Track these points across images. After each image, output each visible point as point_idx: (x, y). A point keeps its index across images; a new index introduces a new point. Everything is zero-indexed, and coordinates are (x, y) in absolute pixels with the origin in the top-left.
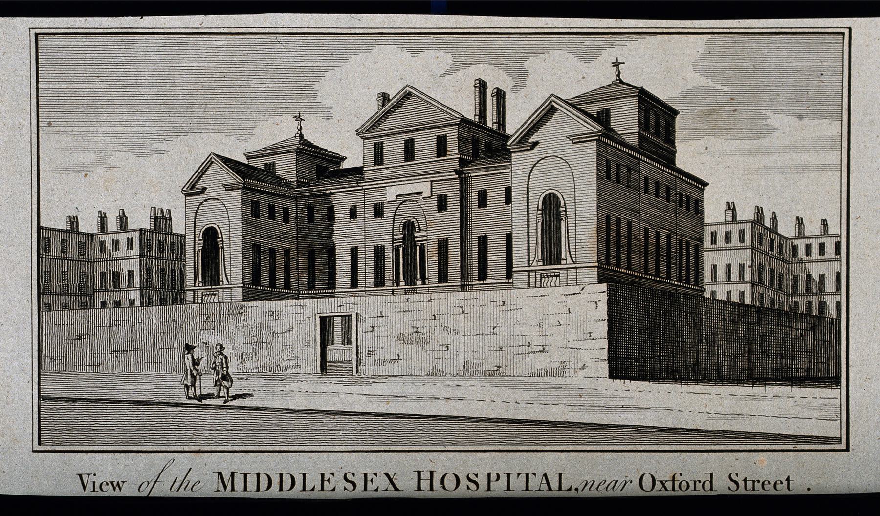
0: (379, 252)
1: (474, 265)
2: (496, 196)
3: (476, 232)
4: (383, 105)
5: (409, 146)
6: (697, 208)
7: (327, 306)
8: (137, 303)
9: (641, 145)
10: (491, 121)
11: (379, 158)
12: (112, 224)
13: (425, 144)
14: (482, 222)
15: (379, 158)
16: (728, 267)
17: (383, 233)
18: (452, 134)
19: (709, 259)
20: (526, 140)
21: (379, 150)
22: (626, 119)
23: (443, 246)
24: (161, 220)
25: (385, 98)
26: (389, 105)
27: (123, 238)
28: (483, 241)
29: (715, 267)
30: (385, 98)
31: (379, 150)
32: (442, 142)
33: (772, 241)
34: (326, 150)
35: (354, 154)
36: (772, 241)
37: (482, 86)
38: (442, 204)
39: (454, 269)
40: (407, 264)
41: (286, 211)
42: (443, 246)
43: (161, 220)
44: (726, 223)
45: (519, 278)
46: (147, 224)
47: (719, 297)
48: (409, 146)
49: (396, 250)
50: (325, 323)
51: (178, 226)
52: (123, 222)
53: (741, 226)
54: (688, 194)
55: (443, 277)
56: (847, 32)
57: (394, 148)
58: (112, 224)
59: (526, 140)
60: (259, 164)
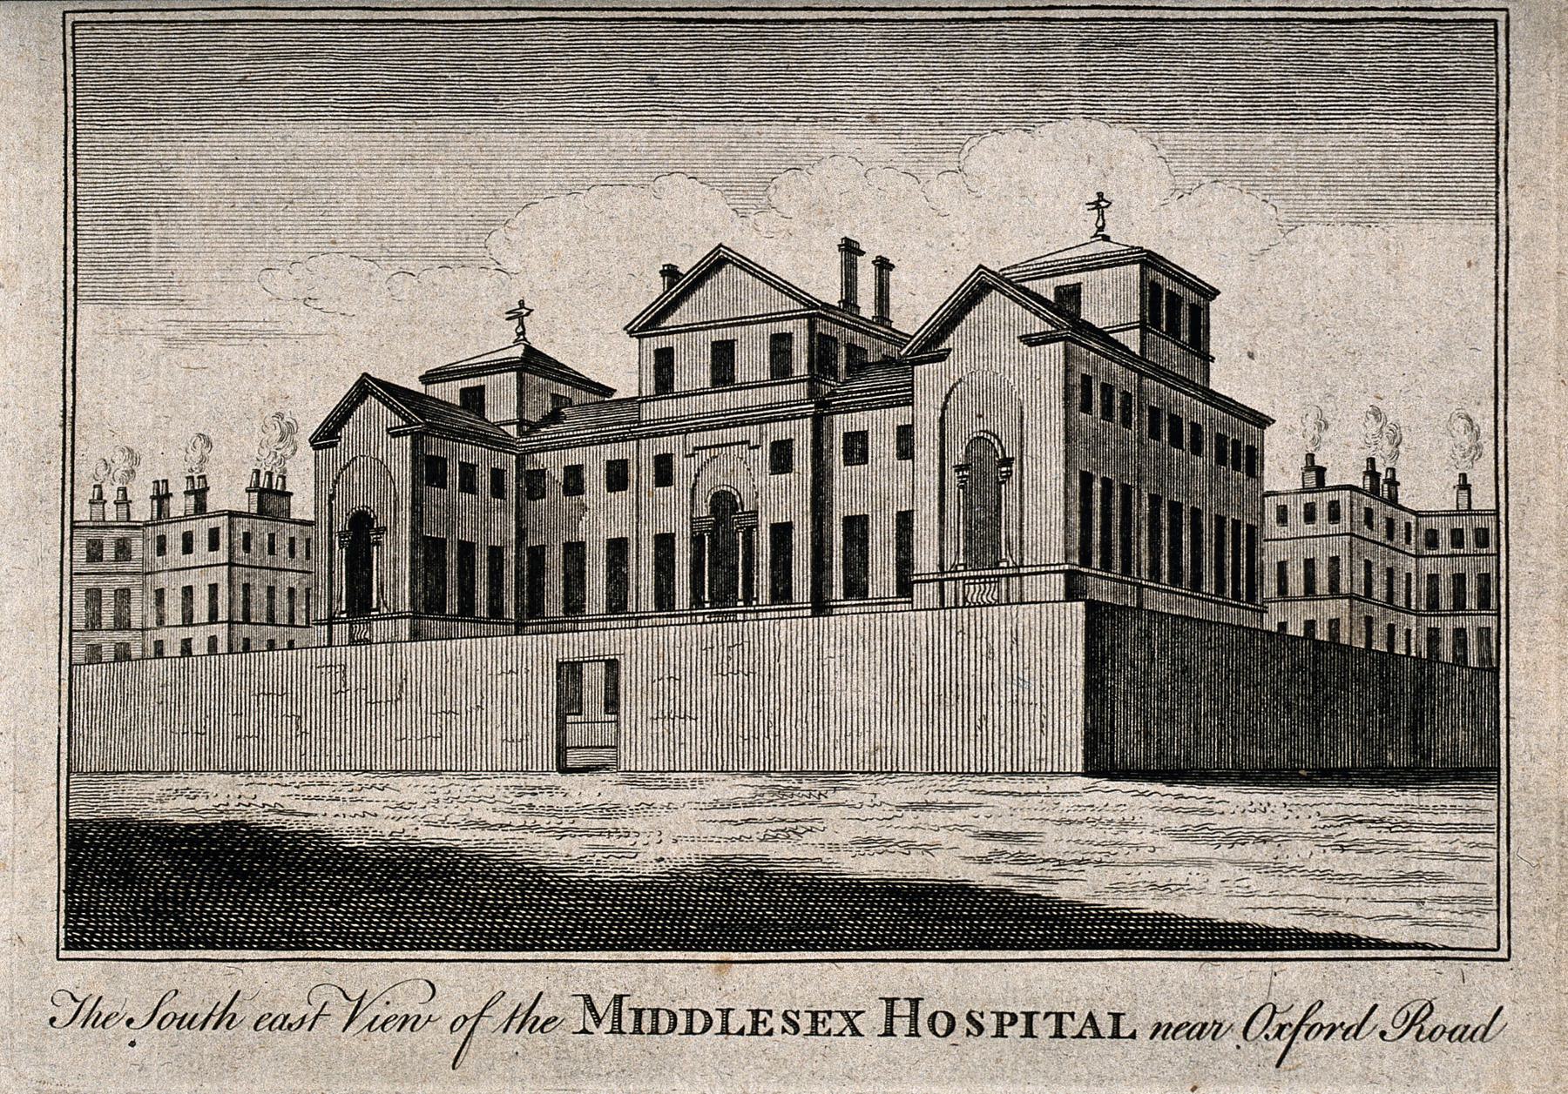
0: (665, 543)
1: (837, 565)
2: (882, 446)
3: (841, 507)
4: (671, 285)
5: (723, 354)
6: (1251, 461)
7: (570, 645)
8: (222, 647)
9: (1146, 348)
10: (867, 309)
11: (664, 385)
12: (179, 504)
13: (752, 360)
14: (851, 490)
15: (664, 385)
16: (1309, 564)
17: (674, 511)
18: (799, 331)
19: (1270, 556)
20: (932, 345)
21: (664, 359)
22: (1110, 302)
23: (782, 533)
24: (270, 498)
25: (670, 273)
26: (680, 285)
27: (200, 529)
28: (856, 527)
29: (1282, 566)
30: (670, 273)
31: (664, 359)
32: (780, 344)
33: (1390, 523)
34: (564, 367)
35: (620, 367)
36: (1390, 523)
37: (850, 249)
38: (781, 458)
39: (802, 587)
40: (723, 565)
41: (498, 476)
42: (782, 533)
43: (270, 498)
44: (1305, 490)
45: (925, 594)
46: (243, 502)
47: (1291, 631)
48: (723, 354)
49: (697, 541)
50: (570, 672)
51: (303, 505)
52: (199, 495)
53: (1333, 496)
54: (1238, 441)
55: (782, 593)
56: (1503, 954)
57: (693, 369)
58: (179, 504)
59: (932, 345)
60: (449, 392)
